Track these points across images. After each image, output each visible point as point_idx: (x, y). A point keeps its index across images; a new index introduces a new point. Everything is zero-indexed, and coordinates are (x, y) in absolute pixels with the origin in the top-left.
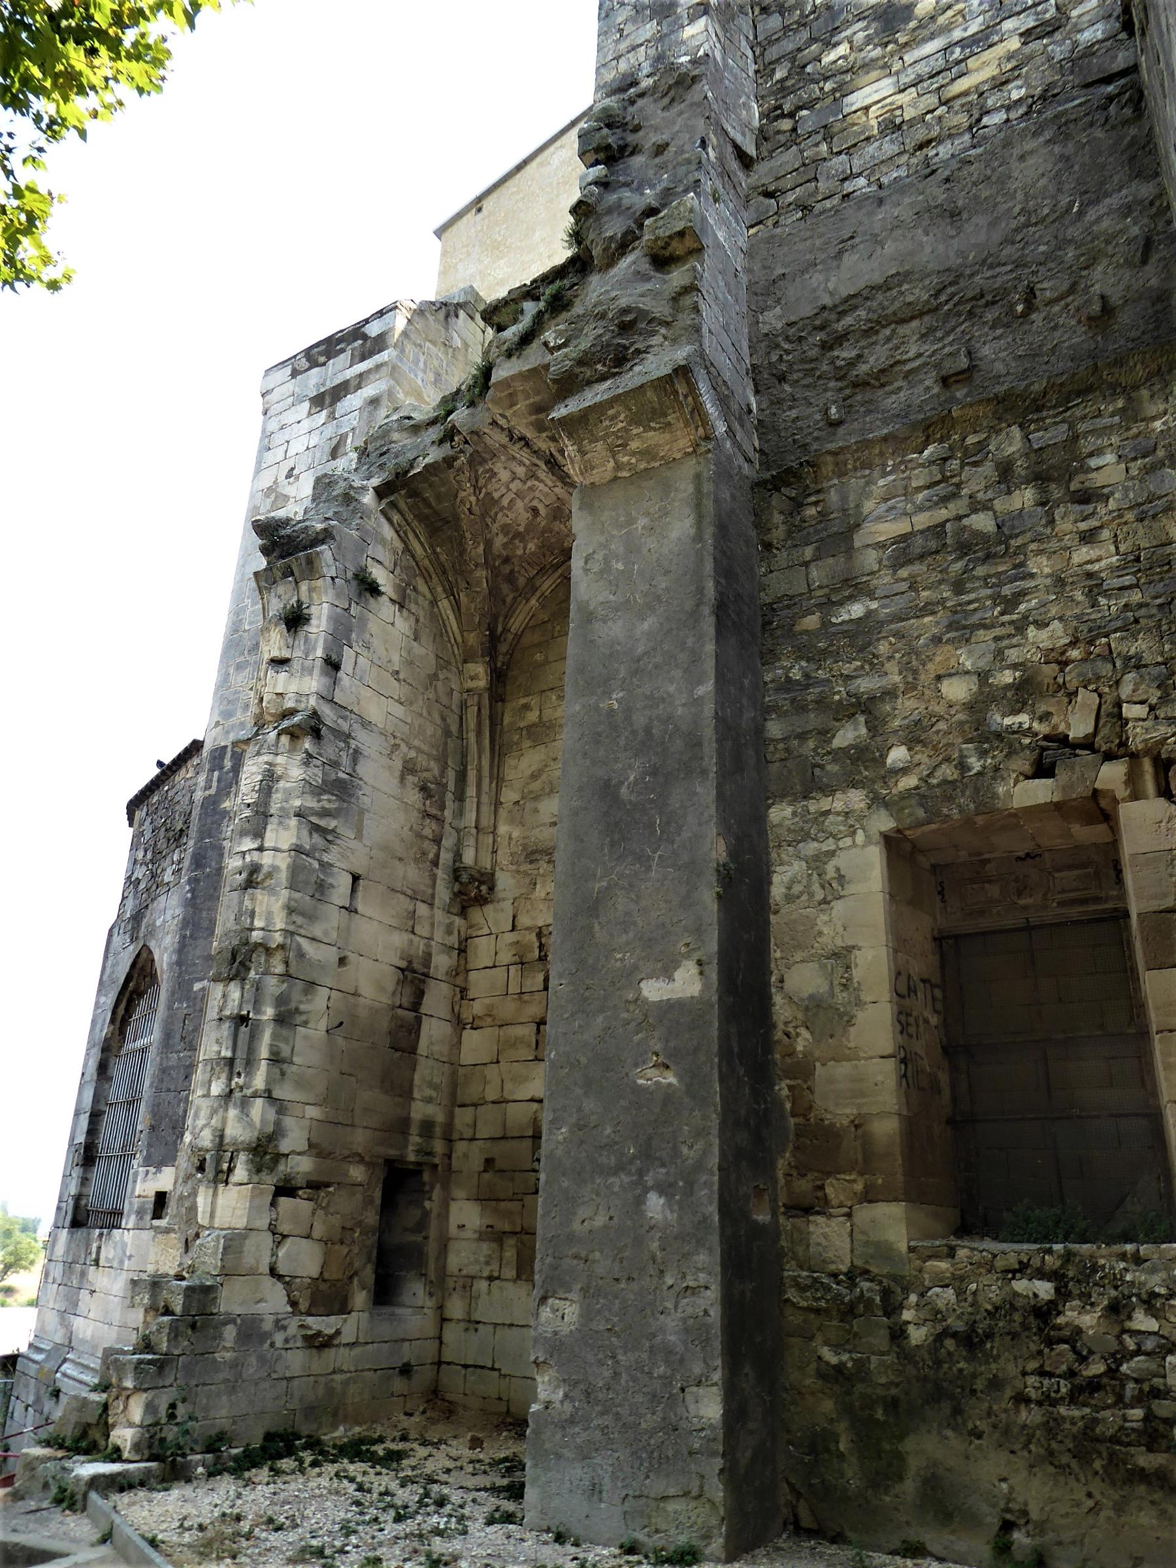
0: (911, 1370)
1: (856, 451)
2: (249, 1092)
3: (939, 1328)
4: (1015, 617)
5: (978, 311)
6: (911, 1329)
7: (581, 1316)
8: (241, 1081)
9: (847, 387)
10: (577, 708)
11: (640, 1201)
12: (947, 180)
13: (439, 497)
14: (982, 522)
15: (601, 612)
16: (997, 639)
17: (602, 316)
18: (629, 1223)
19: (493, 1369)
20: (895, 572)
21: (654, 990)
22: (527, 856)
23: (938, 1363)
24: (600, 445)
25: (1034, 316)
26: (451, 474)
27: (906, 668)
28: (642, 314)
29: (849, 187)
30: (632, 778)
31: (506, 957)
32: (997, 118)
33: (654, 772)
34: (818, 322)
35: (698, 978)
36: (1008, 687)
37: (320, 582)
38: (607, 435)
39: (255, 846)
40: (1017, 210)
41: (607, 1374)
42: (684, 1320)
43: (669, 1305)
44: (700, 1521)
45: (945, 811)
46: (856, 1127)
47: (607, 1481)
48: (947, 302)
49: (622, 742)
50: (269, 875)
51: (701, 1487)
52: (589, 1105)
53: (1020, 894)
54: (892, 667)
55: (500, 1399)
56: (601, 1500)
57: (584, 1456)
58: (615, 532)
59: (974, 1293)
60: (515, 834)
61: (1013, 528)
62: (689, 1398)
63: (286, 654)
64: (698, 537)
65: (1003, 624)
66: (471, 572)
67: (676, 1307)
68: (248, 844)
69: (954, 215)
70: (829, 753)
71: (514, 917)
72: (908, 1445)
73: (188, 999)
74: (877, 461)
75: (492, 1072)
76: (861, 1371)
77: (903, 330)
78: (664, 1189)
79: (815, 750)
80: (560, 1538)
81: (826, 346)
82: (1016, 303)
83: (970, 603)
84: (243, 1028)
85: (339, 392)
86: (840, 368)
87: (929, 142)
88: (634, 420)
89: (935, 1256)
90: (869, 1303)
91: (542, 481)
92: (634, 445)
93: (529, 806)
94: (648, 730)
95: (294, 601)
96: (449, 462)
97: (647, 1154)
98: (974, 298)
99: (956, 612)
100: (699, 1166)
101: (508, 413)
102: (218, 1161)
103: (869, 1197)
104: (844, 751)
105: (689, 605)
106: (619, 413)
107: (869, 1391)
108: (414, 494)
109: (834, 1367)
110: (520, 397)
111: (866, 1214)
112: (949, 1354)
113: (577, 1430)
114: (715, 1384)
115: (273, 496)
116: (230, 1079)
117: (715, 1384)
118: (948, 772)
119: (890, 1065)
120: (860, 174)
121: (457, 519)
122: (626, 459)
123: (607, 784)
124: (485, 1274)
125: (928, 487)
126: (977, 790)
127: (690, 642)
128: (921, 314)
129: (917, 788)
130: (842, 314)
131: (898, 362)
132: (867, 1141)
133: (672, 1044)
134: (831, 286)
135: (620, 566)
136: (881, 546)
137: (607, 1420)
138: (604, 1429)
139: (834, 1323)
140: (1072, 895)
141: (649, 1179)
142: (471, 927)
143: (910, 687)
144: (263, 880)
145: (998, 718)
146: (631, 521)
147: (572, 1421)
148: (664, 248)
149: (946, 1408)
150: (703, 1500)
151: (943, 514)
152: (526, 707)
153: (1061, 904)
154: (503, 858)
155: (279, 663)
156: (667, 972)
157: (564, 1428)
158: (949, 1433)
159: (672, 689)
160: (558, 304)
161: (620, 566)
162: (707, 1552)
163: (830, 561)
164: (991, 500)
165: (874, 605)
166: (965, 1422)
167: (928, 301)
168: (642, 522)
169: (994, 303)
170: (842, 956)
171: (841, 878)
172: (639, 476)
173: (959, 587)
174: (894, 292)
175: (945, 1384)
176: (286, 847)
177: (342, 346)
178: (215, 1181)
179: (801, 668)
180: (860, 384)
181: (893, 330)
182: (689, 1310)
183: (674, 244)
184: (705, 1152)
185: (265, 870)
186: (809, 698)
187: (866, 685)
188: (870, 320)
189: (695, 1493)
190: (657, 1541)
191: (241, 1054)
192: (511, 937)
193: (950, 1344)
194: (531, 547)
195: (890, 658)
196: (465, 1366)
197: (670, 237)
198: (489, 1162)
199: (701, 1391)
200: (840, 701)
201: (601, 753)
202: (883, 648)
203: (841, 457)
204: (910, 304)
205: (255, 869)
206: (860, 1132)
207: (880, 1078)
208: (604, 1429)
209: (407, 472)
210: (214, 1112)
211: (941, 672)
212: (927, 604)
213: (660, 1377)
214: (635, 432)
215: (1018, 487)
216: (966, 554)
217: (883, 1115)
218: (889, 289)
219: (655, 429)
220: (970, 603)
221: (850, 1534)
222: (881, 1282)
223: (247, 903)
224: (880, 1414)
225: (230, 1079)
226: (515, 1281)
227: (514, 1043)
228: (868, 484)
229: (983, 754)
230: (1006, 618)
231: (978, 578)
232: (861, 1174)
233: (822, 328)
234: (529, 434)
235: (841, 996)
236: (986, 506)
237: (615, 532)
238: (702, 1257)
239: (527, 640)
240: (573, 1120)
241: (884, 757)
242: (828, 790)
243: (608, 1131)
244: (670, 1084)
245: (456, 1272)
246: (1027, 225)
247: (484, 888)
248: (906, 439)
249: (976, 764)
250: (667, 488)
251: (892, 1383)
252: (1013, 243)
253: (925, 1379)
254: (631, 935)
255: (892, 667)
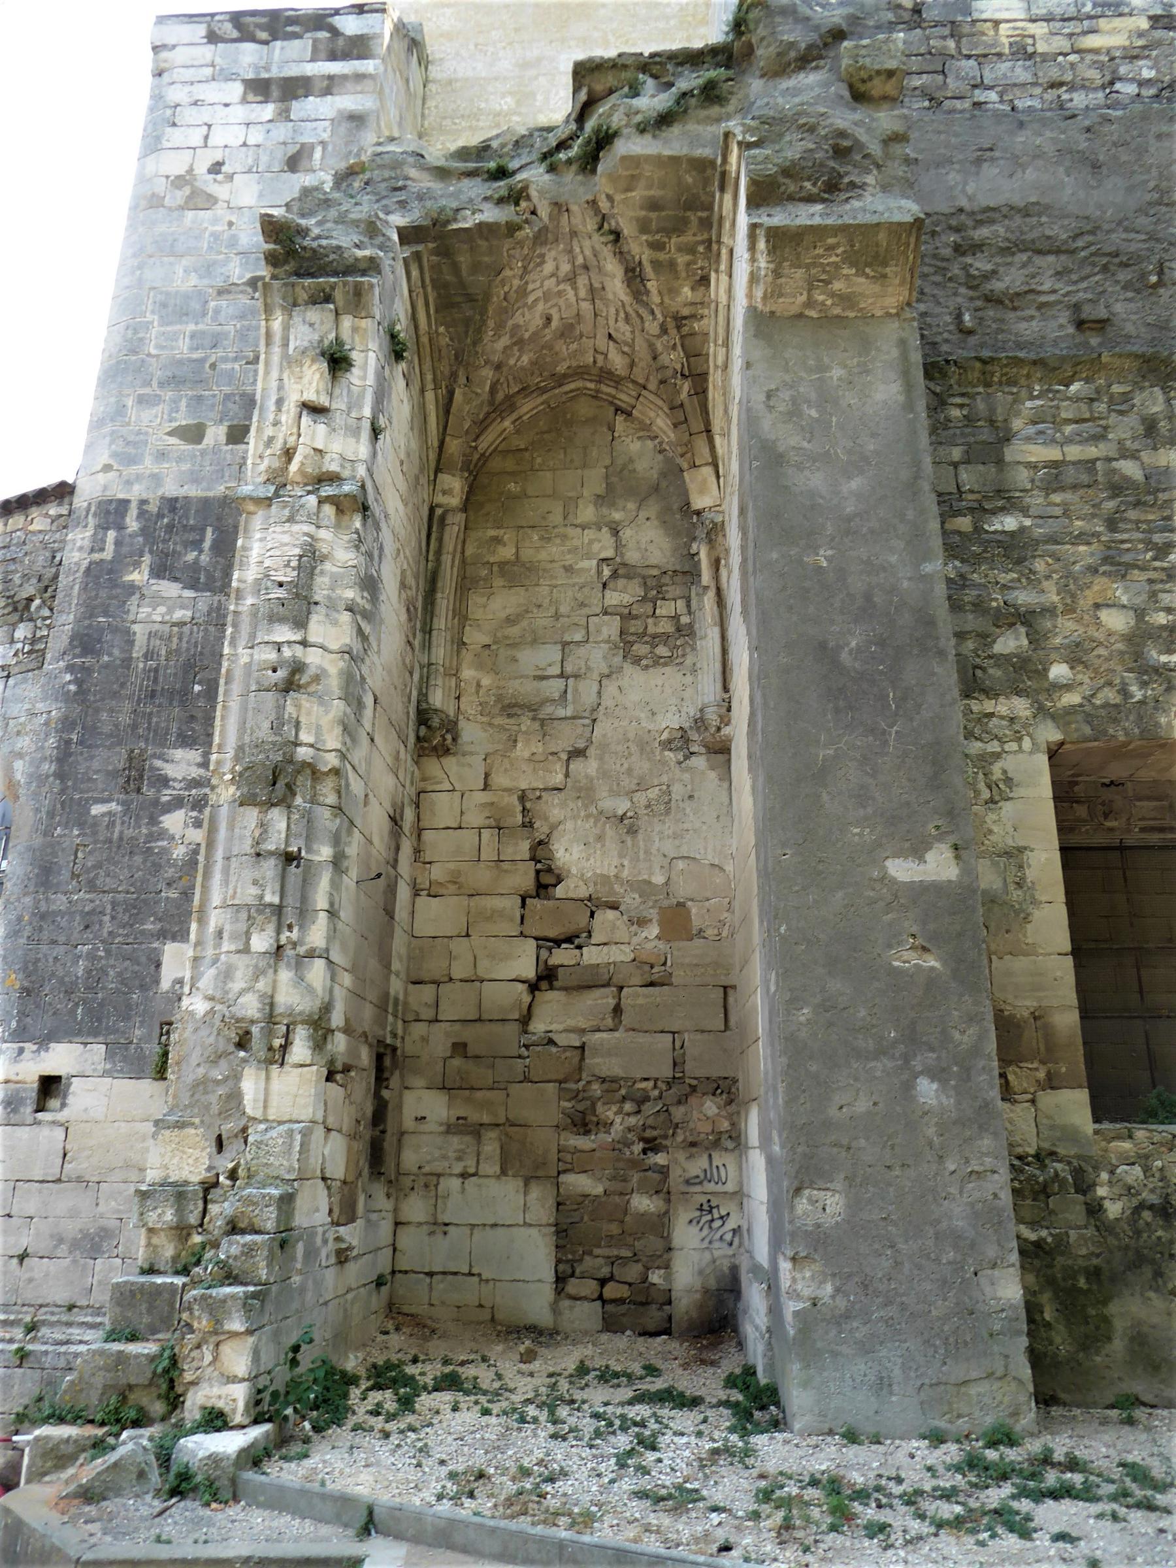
0: (1112, 1241)
1: (1006, 366)
2: (302, 950)
3: (1135, 1202)
4: (1165, 565)
5: (1112, 268)
6: (1107, 1204)
7: (848, 1206)
8: (295, 935)
9: (978, 298)
10: (775, 556)
11: (908, 1087)
12: (1088, 130)
13: (476, 267)
14: (1130, 469)
15: (794, 457)
16: (1151, 581)
17: (812, 129)
18: (898, 1109)
19: (471, 1274)
20: (1047, 495)
21: (901, 870)
22: (503, 708)
23: (1138, 1233)
24: (800, 273)
25: (1162, 291)
26: (507, 244)
27: (1063, 589)
28: (858, 145)
29: (980, 95)
30: (853, 644)
31: (475, 818)
32: (1131, 89)
33: (882, 643)
34: (954, 222)
35: (953, 862)
36: (1163, 628)
37: (364, 323)
38: (814, 265)
39: (298, 637)
40: (1152, 184)
41: (886, 1264)
42: (972, 1205)
43: (953, 1190)
44: (1006, 1399)
45: (1111, 731)
46: (1035, 1018)
47: (897, 1372)
48: (1084, 248)
49: (837, 605)
50: (317, 679)
51: (1006, 1367)
52: (835, 985)
53: (1106, 816)
54: (1050, 586)
55: (481, 1306)
56: (891, 1393)
57: (866, 1349)
58: (803, 374)
59: (1161, 1170)
60: (486, 681)
61: (1159, 482)
62: (983, 1281)
63: (324, 401)
64: (909, 406)
65: (1155, 569)
66: (479, 367)
67: (961, 1192)
68: (284, 633)
69: (1096, 166)
70: (990, 657)
71: (487, 775)
72: (1113, 1308)
73: (81, 825)
74: (1023, 381)
75: (460, 947)
76: (1061, 1244)
77: (1039, 260)
78: (937, 1074)
79: (975, 651)
80: (852, 1437)
81: (958, 249)
82: (1150, 273)
83: (1122, 542)
84: (292, 869)
85: (292, 89)
86: (974, 277)
87: (1061, 84)
88: (852, 259)
89: (1119, 1137)
90: (1063, 1182)
91: (575, 289)
92: (837, 286)
93: (503, 653)
94: (868, 597)
95: (332, 336)
96: (512, 228)
97: (912, 1039)
98: (1109, 254)
99: (1109, 548)
100: (976, 1051)
101: (618, 197)
102: (269, 1034)
103: (1052, 1083)
104: (1006, 658)
105: (905, 474)
106: (838, 245)
107: (1070, 1262)
108: (444, 252)
109: (1032, 1243)
110: (642, 183)
111: (1047, 1099)
112: (1147, 1224)
113: (855, 1324)
114: (1013, 1265)
115: (187, 190)
116: (278, 932)
117: (1013, 1265)
118: (1110, 695)
119: (1069, 961)
120: (991, 88)
121: (487, 297)
122: (821, 298)
123: (823, 646)
124: (458, 1169)
125: (1077, 422)
126: (1140, 718)
127: (910, 514)
128: (1058, 252)
129: (1081, 705)
130: (979, 223)
131: (1032, 291)
132: (1048, 1033)
133: (932, 926)
134: (970, 189)
135: (814, 413)
136: (1033, 466)
137: (892, 1311)
138: (889, 1322)
139: (1029, 1202)
140: (1152, 823)
141: (917, 1064)
142: (424, 779)
143: (1070, 610)
144: (309, 684)
145: (1154, 654)
146: (822, 368)
147: (847, 1316)
148: (864, 81)
149: (1148, 1271)
150: (1009, 1378)
151: (1092, 451)
152: (497, 540)
153: (1143, 830)
154: (469, 705)
155: (316, 410)
156: (918, 851)
157: (839, 1324)
158: (1151, 1294)
159: (893, 559)
160: (711, 94)
161: (814, 413)
162: (1018, 1428)
163: (981, 467)
164: (1138, 451)
165: (1028, 522)
166: (1165, 1283)
167: (1065, 242)
168: (836, 373)
169: (1127, 265)
170: (1015, 855)
171: (1008, 780)
172: (829, 321)
173: (1112, 524)
174: (1034, 220)
175: (1146, 1252)
176: (334, 646)
177: (296, 29)
178: (270, 1062)
179: (955, 567)
180: (992, 299)
181: (1030, 258)
182: (977, 1195)
183: (876, 82)
184: (981, 1037)
185: (312, 671)
186: (966, 599)
187: (1024, 598)
188: (1007, 239)
189: (999, 1374)
190: (963, 1424)
191: (292, 901)
192: (482, 797)
193: (1147, 1215)
194: (525, 359)
195: (1048, 577)
196: (430, 1274)
197: (878, 72)
198: (460, 1048)
199: (996, 1272)
200: (998, 609)
201: (811, 609)
202: (1039, 566)
203: (989, 368)
204: (1049, 238)
205: (298, 668)
206: (1039, 1023)
207: (1059, 974)
208: (889, 1322)
209: (448, 222)
210: (258, 974)
211: (1099, 601)
212: (1081, 534)
213: (949, 1263)
214: (845, 272)
215: (1163, 446)
216: (1117, 496)
217: (1065, 1008)
218: (1028, 215)
219: (867, 276)
220: (1122, 542)
221: (1063, 1396)
222: (1069, 1163)
223: (290, 709)
224: (1082, 1283)
225: (278, 932)
226: (498, 1177)
227: (492, 916)
228: (1015, 401)
229: (1144, 685)
230: (1157, 564)
231: (1131, 521)
232: (1043, 1062)
233: (957, 230)
234: (627, 230)
235: (1016, 895)
236: (1134, 456)
237: (803, 374)
238: (986, 1142)
239: (496, 464)
240: (817, 1000)
241: (1046, 670)
242: (990, 693)
243: (863, 1013)
244: (932, 968)
245: (415, 1170)
246: (1159, 203)
247: (449, 737)
248: (1055, 369)
249: (1138, 695)
250: (866, 344)
251: (1092, 1254)
252: (1147, 215)
253: (1127, 1247)
254: (870, 810)
255: (1050, 586)
